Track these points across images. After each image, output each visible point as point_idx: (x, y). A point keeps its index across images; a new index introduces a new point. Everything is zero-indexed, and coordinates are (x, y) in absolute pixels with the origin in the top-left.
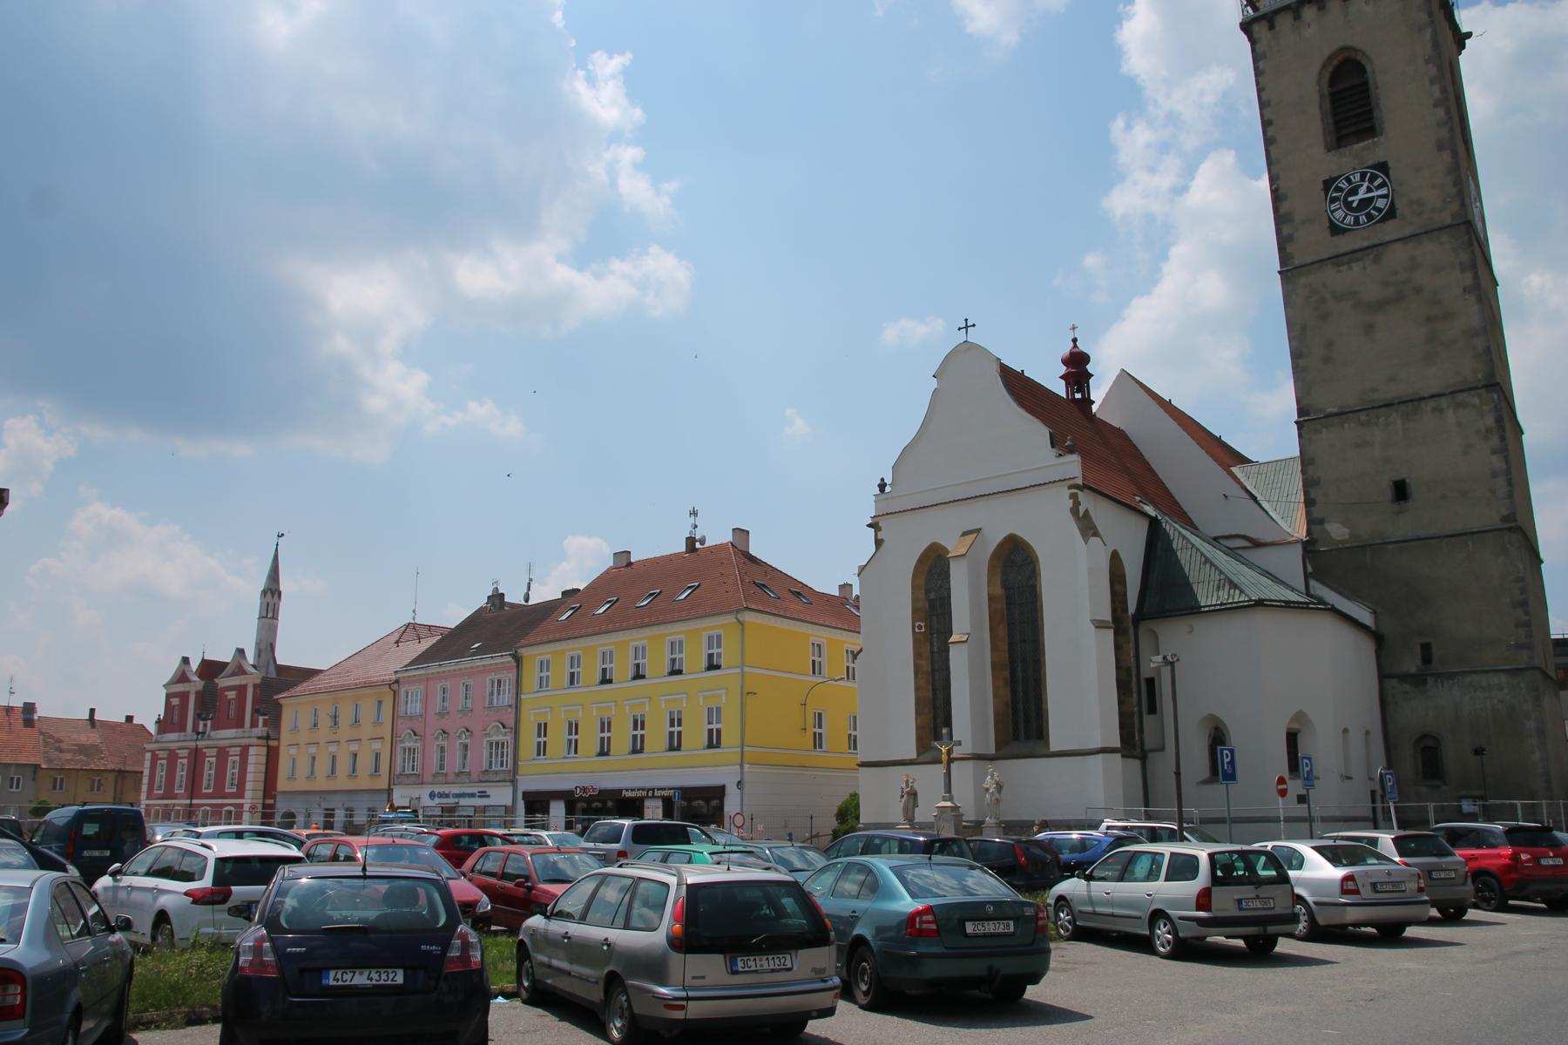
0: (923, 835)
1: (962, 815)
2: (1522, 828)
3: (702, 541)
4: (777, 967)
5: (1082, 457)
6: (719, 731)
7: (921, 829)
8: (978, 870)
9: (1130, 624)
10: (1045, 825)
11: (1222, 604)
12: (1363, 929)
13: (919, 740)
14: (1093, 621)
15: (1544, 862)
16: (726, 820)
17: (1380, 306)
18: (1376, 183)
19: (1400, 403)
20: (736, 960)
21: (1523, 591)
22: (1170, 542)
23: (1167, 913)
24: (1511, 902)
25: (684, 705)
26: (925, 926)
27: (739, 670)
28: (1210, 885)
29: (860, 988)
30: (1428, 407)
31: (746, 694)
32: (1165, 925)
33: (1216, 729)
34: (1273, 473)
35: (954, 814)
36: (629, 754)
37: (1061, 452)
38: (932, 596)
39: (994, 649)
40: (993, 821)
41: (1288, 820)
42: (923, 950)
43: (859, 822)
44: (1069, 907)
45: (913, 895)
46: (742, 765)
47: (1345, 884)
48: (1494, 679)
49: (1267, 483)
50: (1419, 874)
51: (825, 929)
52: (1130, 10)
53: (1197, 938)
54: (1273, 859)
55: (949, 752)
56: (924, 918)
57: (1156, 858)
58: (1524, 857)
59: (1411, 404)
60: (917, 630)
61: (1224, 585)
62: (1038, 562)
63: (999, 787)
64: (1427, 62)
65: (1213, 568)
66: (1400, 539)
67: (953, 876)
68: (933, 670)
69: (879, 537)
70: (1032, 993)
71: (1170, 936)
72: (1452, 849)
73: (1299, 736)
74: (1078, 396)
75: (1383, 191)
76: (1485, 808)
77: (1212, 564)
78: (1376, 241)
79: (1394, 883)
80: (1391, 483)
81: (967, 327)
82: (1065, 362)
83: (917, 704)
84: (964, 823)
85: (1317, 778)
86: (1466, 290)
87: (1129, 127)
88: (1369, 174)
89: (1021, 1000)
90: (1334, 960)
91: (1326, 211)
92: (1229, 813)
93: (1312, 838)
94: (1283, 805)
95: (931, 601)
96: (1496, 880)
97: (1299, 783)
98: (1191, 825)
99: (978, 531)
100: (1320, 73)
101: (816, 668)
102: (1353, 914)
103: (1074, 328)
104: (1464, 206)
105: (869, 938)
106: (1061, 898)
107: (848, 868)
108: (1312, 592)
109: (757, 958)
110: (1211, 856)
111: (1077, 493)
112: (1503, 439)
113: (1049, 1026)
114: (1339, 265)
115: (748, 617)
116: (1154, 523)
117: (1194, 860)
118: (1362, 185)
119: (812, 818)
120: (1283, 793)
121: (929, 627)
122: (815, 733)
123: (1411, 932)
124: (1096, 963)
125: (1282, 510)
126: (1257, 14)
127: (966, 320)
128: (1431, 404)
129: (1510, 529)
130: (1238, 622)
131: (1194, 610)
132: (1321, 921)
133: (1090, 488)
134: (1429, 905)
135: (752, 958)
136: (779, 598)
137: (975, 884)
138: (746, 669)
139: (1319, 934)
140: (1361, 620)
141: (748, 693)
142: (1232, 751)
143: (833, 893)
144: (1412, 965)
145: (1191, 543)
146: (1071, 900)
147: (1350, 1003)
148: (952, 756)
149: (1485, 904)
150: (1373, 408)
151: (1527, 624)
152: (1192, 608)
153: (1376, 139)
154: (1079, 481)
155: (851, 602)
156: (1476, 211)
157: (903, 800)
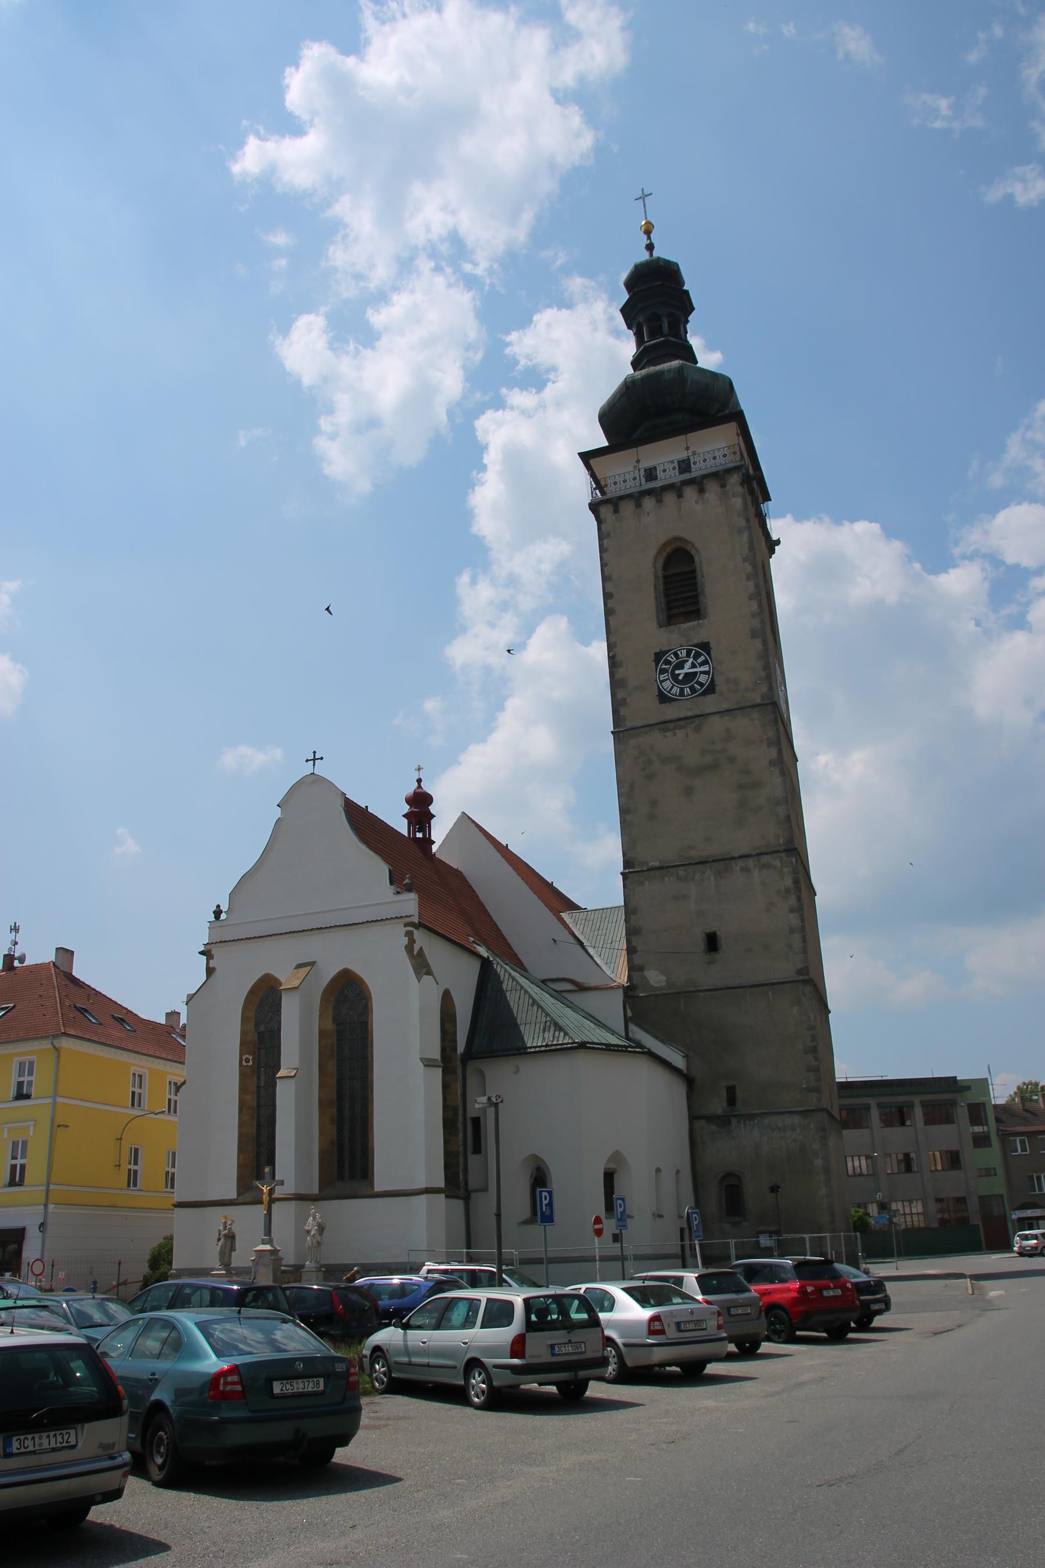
0: (236, 1283)
1: (282, 1259)
2: (808, 1262)
3: (22, 959)
4: (59, 1445)
5: (419, 895)
6: (23, 1167)
7: (237, 1274)
8: (290, 1324)
9: (459, 1063)
10: (368, 1270)
11: (547, 1046)
12: (668, 1368)
13: (241, 1178)
14: (422, 1060)
15: (826, 1293)
16: (24, 1268)
17: (699, 771)
18: (699, 660)
19: (713, 861)
20: (12, 1439)
21: (814, 1038)
22: (501, 983)
23: (481, 1362)
24: (798, 1333)
25: (31, 1133)
26: (229, 1388)
27: (50, 1101)
28: (524, 1332)
29: (154, 1460)
30: (737, 866)
31: (57, 1126)
32: (480, 1374)
33: (538, 1169)
34: (599, 920)
35: (272, 1258)
36: (5, 1186)
37: (399, 890)
38: (262, 1028)
39: (322, 1085)
40: (313, 1265)
41: (603, 1259)
42: (226, 1414)
43: (171, 1269)
44: (385, 1358)
45: (219, 1354)
46: (46, 1206)
47: (652, 1324)
48: (789, 1120)
49: (593, 929)
50: (719, 1312)
51: (117, 1398)
52: (482, 477)
53: (511, 1387)
54: (586, 1303)
55: (271, 1192)
56: (230, 1379)
57: (473, 1304)
58: (810, 1289)
59: (723, 862)
60: (244, 1063)
61: (550, 1026)
62: (371, 998)
63: (321, 1229)
64: (744, 560)
65: (540, 1010)
66: (710, 988)
67: (261, 1330)
68: (259, 1106)
69: (211, 965)
70: (341, 1456)
71: (484, 1386)
72: (748, 1285)
73: (615, 1175)
74: (419, 835)
75: (705, 668)
76: (779, 1243)
77: (539, 1006)
78: (698, 712)
79: (698, 1322)
80: (704, 935)
81: (314, 759)
82: (409, 801)
83: (240, 1141)
84: (283, 1268)
85: (630, 1217)
86: (772, 763)
87: (474, 582)
88: (694, 652)
89: (329, 1465)
90: (641, 1402)
91: (656, 680)
92: (546, 1254)
93: (624, 1279)
94: (599, 1245)
95: (261, 1035)
96: (787, 1313)
97: (613, 1221)
98: (510, 1267)
99: (312, 964)
100: (656, 557)
101: (135, 1100)
102: (659, 1355)
103: (419, 769)
104: (771, 688)
105: (168, 1402)
106: (377, 1349)
107: (149, 1326)
108: (631, 1035)
109: (37, 1436)
110: (526, 1301)
111: (412, 932)
112: (799, 899)
113: (356, 1493)
114: (665, 730)
115: (66, 1043)
116: (486, 965)
117: (510, 1305)
118: (687, 661)
119: (120, 1264)
120: (599, 1233)
121: (257, 1060)
122: (130, 1170)
123: (711, 1368)
124: (409, 1418)
125: (606, 955)
126: (605, 498)
127: (315, 752)
128: (740, 863)
129: (804, 981)
130: (562, 1065)
131: (520, 1050)
132: (630, 1363)
133: (426, 927)
134: (727, 1342)
135: (30, 1437)
136: (101, 1024)
137: (283, 1337)
138: (59, 1100)
139: (629, 1376)
140: (674, 1064)
141: (59, 1126)
142: (550, 1193)
143: (132, 1352)
144: (710, 1403)
145: (520, 985)
146: (387, 1350)
147: (652, 1447)
148: (273, 1196)
149: (777, 1337)
150: (690, 864)
151: (816, 1070)
152: (518, 1049)
153: (700, 621)
154: (416, 920)
155: (178, 1031)
156: (781, 694)
157: (220, 1243)
